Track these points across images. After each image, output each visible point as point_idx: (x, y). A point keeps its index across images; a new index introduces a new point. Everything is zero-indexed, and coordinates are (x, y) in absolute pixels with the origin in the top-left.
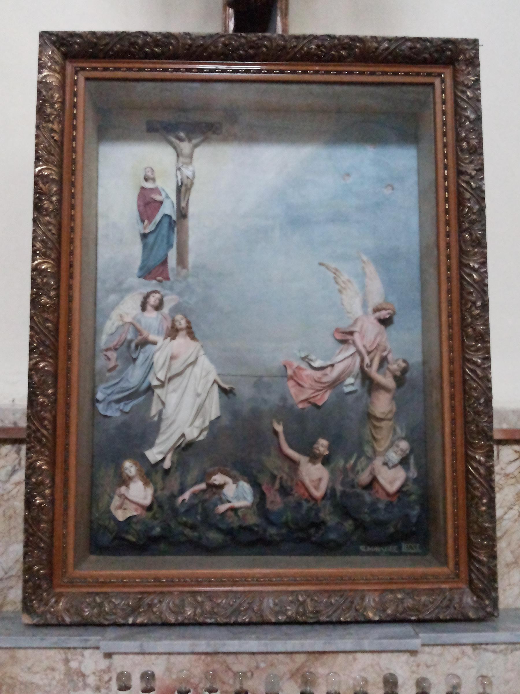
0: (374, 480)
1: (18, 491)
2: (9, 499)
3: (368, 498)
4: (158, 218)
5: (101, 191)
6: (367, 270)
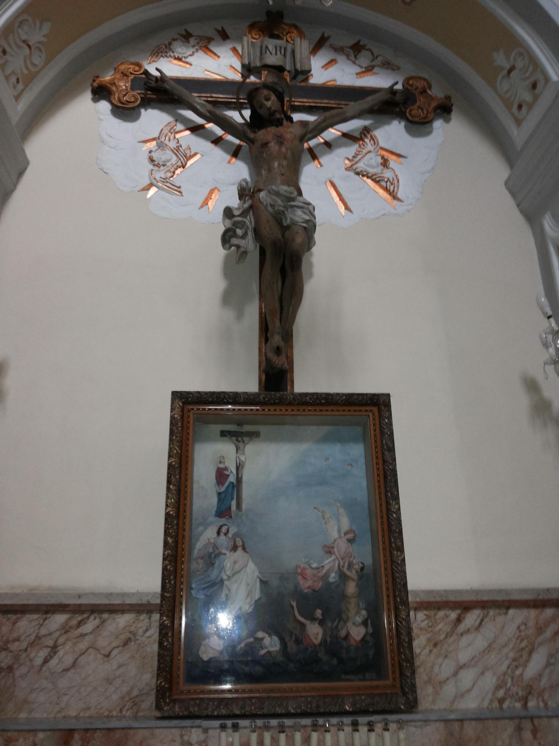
0: (348, 634)
1: (149, 642)
2: (143, 647)
3: (345, 644)
4: (227, 484)
5: (195, 469)
6: (340, 512)
